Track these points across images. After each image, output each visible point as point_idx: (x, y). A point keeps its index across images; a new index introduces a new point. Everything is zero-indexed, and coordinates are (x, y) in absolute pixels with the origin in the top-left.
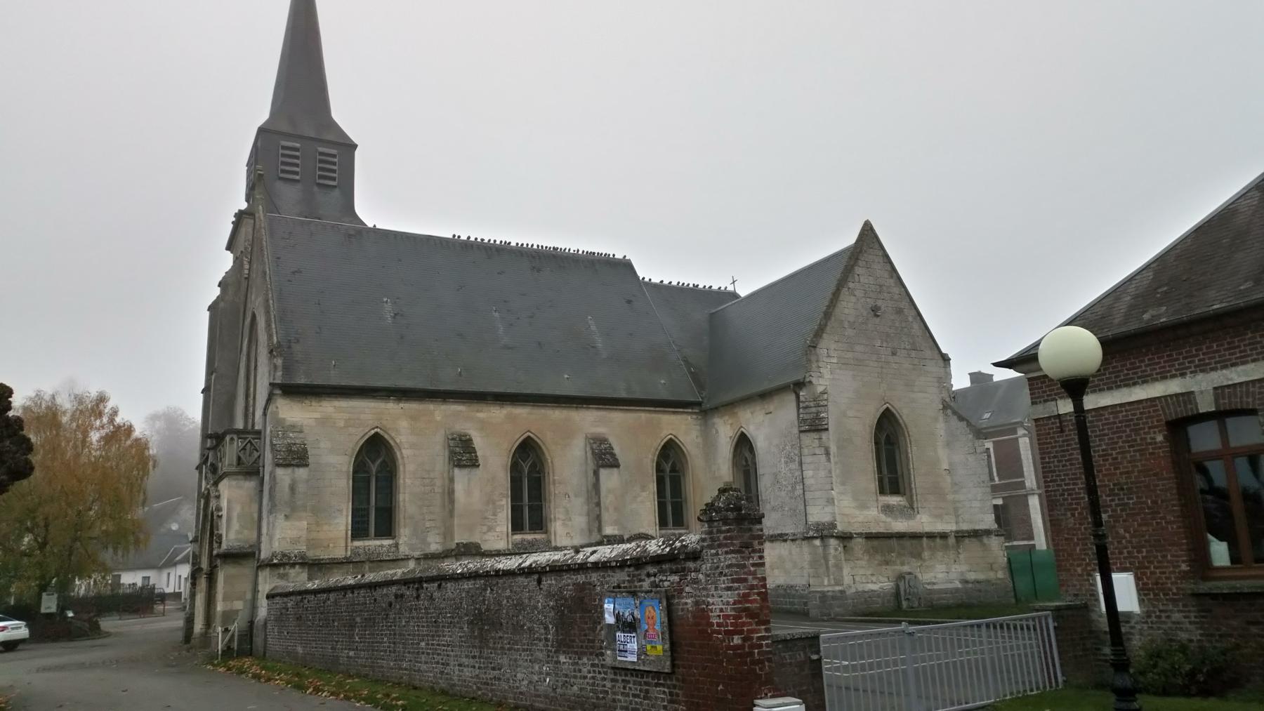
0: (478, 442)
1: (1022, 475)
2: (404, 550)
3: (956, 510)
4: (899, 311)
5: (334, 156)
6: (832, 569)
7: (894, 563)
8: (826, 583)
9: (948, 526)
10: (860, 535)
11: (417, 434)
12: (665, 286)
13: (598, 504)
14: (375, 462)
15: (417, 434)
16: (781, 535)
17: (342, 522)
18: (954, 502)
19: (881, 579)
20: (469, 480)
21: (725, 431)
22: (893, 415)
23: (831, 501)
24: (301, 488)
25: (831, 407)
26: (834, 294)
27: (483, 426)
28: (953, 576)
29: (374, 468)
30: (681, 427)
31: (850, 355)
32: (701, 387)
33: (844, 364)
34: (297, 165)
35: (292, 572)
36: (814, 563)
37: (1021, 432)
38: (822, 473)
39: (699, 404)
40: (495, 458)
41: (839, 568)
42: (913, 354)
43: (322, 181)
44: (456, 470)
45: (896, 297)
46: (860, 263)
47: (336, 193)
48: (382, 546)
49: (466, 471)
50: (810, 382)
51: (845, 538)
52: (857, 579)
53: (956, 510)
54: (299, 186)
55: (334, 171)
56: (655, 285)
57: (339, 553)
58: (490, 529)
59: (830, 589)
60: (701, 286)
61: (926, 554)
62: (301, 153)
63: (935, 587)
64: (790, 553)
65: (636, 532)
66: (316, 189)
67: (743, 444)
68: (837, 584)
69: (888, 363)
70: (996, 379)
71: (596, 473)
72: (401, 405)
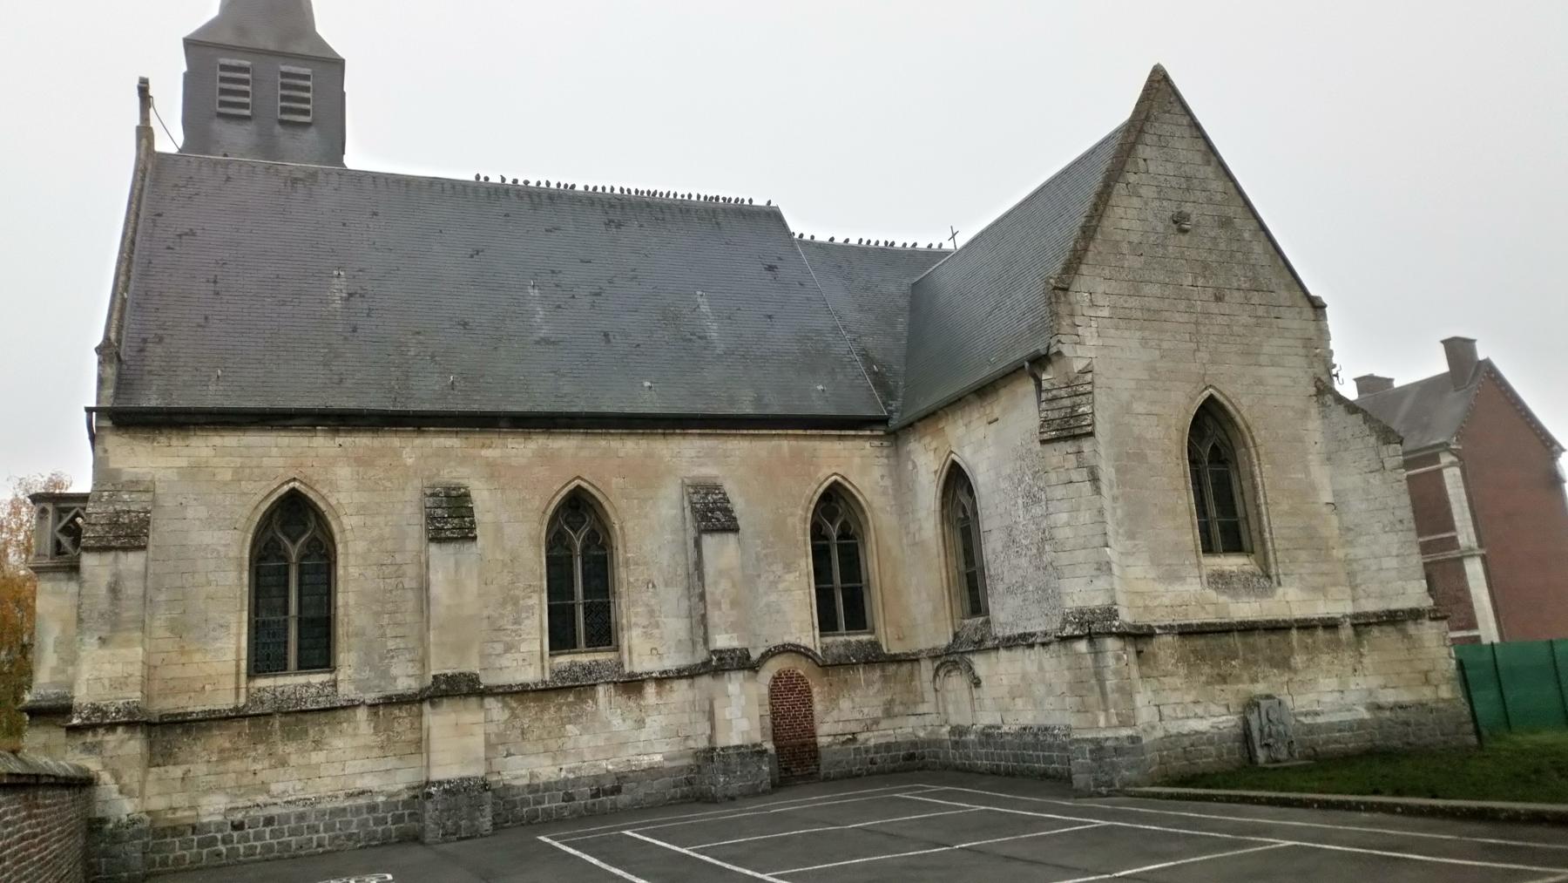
0: (483, 499)
1: (1452, 528)
2: (346, 690)
3: (1351, 575)
4: (1226, 223)
5: (306, 77)
6: (1113, 697)
7: (1238, 679)
8: (1102, 723)
9: (1337, 606)
10: (1168, 629)
11: (366, 491)
12: (839, 246)
13: (702, 597)
14: (292, 541)
15: (366, 491)
16: (1023, 636)
17: (230, 644)
18: (1348, 561)
19: (1214, 709)
20: (457, 564)
21: (925, 463)
22: (1222, 407)
23: (1104, 568)
24: (132, 588)
25: (1100, 397)
26: (1099, 195)
27: (493, 472)
28: (1351, 698)
29: (294, 552)
30: (854, 462)
31: (1133, 302)
32: (888, 393)
33: (1122, 318)
34: (246, 94)
35: (111, 740)
36: (1077, 686)
37: (1446, 459)
38: (1085, 517)
39: (883, 421)
40: (513, 528)
41: (1127, 693)
42: (1256, 298)
43: (286, 117)
44: (433, 548)
45: (1219, 197)
46: (1148, 138)
47: (311, 135)
48: (308, 685)
49: (450, 548)
50: (1059, 353)
51: (1138, 636)
52: (1166, 711)
53: (1351, 575)
54: (250, 126)
55: (307, 101)
56: (821, 245)
57: (224, 700)
58: (509, 648)
59: (1109, 734)
60: (898, 245)
61: (1298, 660)
62: (263, 81)
63: (1320, 720)
64: (1041, 668)
65: (779, 642)
66: (278, 129)
67: (956, 480)
68: (1123, 724)
69: (1208, 314)
70: (1396, 384)
71: (698, 544)
72: (339, 440)
